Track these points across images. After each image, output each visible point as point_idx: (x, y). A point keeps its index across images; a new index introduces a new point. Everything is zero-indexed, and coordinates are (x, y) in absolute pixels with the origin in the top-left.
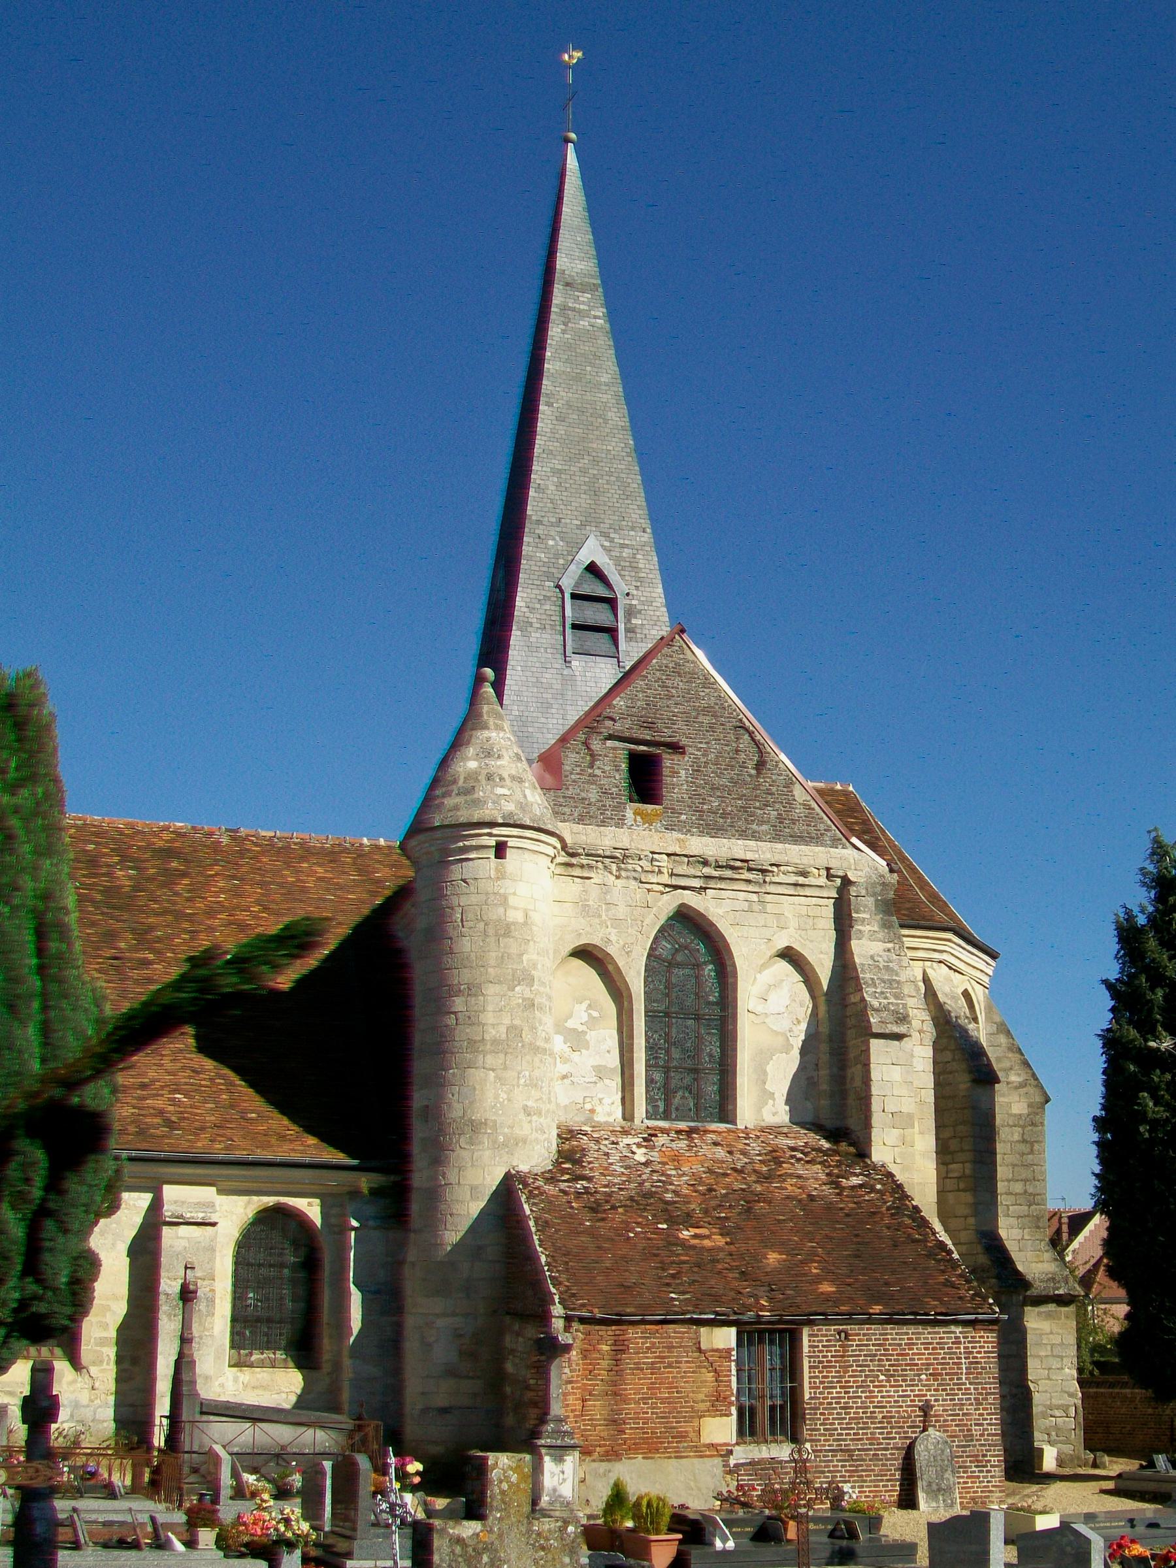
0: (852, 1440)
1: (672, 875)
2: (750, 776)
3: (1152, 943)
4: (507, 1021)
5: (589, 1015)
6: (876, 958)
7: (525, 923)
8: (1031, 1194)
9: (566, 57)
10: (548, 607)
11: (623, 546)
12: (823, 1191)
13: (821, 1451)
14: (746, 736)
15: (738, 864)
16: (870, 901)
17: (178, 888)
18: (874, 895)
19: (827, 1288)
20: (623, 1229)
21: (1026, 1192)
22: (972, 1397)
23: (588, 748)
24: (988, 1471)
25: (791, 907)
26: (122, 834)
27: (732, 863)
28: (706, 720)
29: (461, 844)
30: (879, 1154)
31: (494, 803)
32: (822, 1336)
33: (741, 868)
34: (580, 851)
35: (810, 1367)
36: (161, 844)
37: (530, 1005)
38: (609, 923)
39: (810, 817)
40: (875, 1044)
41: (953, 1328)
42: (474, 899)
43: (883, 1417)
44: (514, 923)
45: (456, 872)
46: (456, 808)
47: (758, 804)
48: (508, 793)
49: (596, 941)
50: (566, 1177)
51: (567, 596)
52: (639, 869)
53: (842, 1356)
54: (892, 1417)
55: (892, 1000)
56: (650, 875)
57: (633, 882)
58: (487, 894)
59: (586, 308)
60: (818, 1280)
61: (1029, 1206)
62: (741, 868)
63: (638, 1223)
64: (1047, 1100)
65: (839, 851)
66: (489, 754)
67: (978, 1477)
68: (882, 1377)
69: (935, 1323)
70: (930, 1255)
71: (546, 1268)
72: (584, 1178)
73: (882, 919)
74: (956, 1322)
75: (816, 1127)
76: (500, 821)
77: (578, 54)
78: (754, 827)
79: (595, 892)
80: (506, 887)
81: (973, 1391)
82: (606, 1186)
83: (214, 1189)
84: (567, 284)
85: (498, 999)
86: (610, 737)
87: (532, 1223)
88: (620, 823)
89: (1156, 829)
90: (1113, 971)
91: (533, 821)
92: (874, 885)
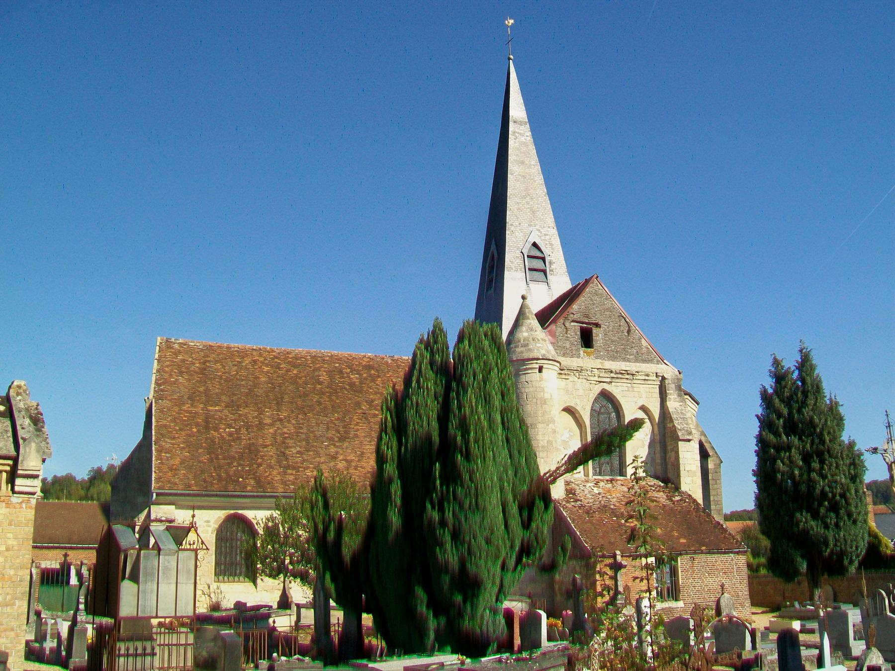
0: (697, 599)
1: (599, 377)
2: (626, 336)
3: (777, 401)
4: (547, 438)
5: (570, 434)
6: (677, 409)
7: (551, 399)
8: (716, 501)
9: (507, 22)
10: (518, 261)
11: (545, 235)
12: (667, 503)
13: (686, 603)
14: (623, 320)
15: (624, 372)
16: (673, 386)
17: (377, 382)
18: (674, 383)
19: (683, 541)
20: (601, 520)
21: (714, 500)
22: (738, 581)
23: (565, 326)
24: (746, 609)
25: (643, 389)
26: (348, 359)
27: (621, 372)
28: (608, 313)
29: (525, 367)
30: (684, 487)
31: (537, 350)
32: (685, 559)
33: (625, 374)
34: (565, 368)
35: (681, 571)
36: (364, 363)
37: (554, 432)
38: (576, 397)
39: (649, 353)
40: (680, 443)
41: (731, 555)
42: (531, 389)
43: (708, 590)
44: (547, 399)
45: (523, 378)
46: (522, 352)
47: (629, 347)
48: (542, 346)
49: (572, 405)
50: (572, 500)
51: (526, 257)
52: (587, 375)
53: (692, 567)
54: (711, 590)
55: (685, 426)
56: (591, 377)
57: (585, 381)
58: (536, 387)
59: (523, 132)
60: (679, 538)
61: (716, 506)
62: (625, 374)
63: (605, 518)
64: (722, 462)
65: (660, 366)
66: (532, 330)
67: (742, 611)
68: (707, 574)
69: (725, 553)
70: (715, 527)
71: (581, 537)
72: (579, 500)
73: (678, 393)
74: (732, 552)
75: (656, 477)
76: (541, 358)
77: (511, 21)
78: (628, 356)
79: (570, 385)
80: (543, 384)
81: (738, 578)
82: (588, 503)
83: (174, 506)
84: (515, 122)
85: (543, 429)
86: (573, 321)
87: (569, 519)
88: (579, 357)
89: (774, 354)
90: (759, 411)
91: (552, 357)
92: (674, 379)
